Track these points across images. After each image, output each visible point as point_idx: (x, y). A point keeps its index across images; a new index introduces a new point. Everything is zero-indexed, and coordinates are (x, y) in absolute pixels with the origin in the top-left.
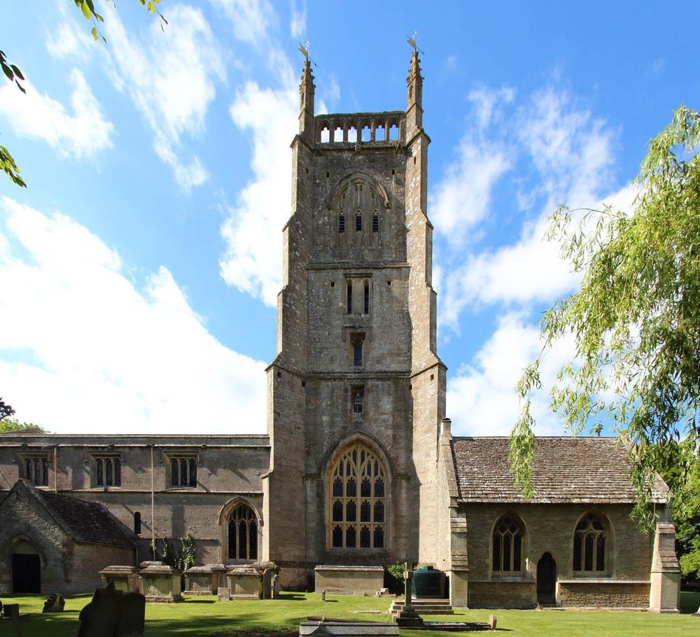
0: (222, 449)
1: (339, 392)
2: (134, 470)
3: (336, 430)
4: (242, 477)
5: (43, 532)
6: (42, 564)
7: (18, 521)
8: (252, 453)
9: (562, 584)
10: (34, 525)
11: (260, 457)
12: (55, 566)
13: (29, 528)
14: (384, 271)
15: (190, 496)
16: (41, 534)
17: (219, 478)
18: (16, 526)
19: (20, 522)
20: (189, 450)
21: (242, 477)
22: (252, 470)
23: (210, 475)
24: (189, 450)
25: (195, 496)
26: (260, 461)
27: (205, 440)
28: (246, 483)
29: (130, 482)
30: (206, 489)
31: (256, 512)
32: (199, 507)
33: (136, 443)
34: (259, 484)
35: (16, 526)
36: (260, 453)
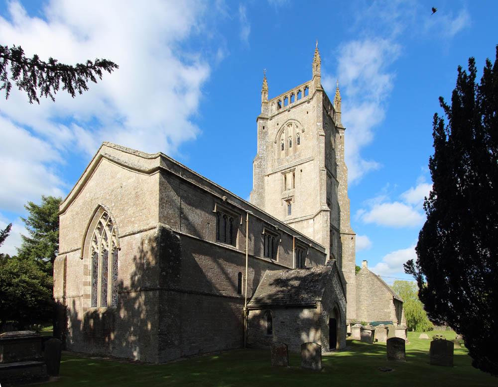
20: (304, 245)
30: (198, 236)
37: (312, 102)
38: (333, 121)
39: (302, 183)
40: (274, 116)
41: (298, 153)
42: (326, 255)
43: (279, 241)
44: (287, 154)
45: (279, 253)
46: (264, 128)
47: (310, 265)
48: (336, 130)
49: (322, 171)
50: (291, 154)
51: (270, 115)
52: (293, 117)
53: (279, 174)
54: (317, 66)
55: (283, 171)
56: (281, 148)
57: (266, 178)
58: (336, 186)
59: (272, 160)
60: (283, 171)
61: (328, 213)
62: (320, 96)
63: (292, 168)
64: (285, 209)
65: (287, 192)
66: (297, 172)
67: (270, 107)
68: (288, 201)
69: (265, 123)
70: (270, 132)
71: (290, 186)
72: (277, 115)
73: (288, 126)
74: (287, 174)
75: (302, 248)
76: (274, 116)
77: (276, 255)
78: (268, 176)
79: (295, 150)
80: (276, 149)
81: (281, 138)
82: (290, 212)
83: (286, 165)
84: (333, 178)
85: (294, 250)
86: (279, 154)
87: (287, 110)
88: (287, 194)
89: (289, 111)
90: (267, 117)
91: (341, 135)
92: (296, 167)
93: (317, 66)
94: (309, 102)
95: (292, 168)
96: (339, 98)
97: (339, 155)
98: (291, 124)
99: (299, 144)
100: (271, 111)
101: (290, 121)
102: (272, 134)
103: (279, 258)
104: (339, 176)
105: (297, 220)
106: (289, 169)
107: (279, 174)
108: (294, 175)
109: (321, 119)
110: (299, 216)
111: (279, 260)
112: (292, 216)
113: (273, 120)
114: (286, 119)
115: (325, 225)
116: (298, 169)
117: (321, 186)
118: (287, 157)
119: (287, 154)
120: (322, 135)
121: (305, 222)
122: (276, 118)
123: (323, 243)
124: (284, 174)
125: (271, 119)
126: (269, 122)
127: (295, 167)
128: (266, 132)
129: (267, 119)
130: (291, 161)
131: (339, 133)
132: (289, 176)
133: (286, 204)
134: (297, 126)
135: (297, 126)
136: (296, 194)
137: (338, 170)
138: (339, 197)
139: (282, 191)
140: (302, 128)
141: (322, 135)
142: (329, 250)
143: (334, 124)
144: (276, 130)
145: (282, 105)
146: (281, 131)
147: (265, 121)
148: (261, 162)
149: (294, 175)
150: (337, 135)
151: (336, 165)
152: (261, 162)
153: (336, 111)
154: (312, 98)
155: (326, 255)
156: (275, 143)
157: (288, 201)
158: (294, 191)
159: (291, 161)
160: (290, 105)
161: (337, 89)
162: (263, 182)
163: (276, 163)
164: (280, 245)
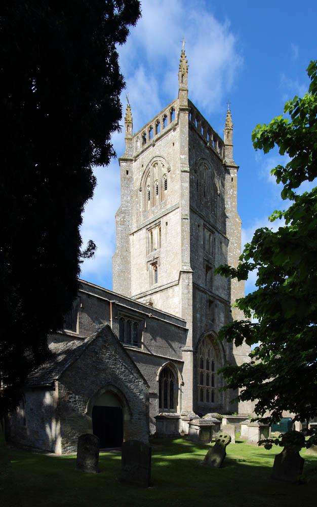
0: (160, 322)
1: (204, 301)
2: (92, 319)
3: (203, 325)
4: (171, 347)
5: (129, 385)
6: (126, 417)
7: (104, 370)
8: (176, 330)
9: (311, 425)
10: (121, 377)
11: (181, 335)
12: (139, 419)
13: (116, 378)
14: (220, 235)
15: (139, 354)
16: (127, 386)
17: (158, 344)
18: (103, 375)
19: (107, 372)
20: (138, 315)
21: (171, 347)
22: (177, 343)
23: (151, 340)
24: (138, 315)
25: (142, 355)
26: (180, 338)
27: (148, 309)
28: (173, 353)
29: (88, 330)
30: (149, 351)
31: (173, 371)
32: (144, 364)
33: (92, 292)
34: (181, 355)
35: (103, 375)
36: (180, 331)
37: (178, 129)
38: (219, 158)
39: (168, 240)
40: (138, 156)
41: (163, 202)
42: (186, 330)
43: (78, 306)
44: (153, 204)
45: (79, 322)
46: (127, 173)
47: (153, 341)
48: (226, 169)
49: (184, 220)
50: (157, 203)
51: (135, 154)
52: (158, 153)
53: (144, 230)
54: (183, 75)
55: (149, 226)
56: (147, 198)
57: (131, 237)
58: (223, 244)
59: (137, 213)
60: (149, 226)
61: (191, 276)
62: (185, 117)
63: (157, 222)
64: (151, 276)
65: (154, 252)
66: (163, 225)
67: (134, 145)
68: (154, 264)
69: (129, 166)
70: (135, 178)
71: (156, 245)
72: (142, 152)
73: (154, 166)
74: (153, 230)
75: (134, 318)
76: (138, 156)
77: (76, 323)
78: (133, 234)
79: (162, 199)
80: (141, 198)
81: (148, 184)
82: (156, 281)
83: (151, 218)
84: (216, 233)
85: (111, 319)
86: (145, 205)
87: (151, 145)
88: (153, 254)
89: (154, 146)
90: (130, 158)
91: (232, 175)
92: (161, 220)
93: (183, 75)
94: (175, 129)
95: (157, 222)
96: (231, 124)
97: (229, 203)
98: (157, 163)
99: (166, 188)
100: (136, 149)
101: (155, 159)
102: (137, 179)
103: (80, 328)
104: (228, 230)
105: (162, 288)
106: (154, 223)
107: (144, 230)
108: (160, 230)
109: (187, 149)
110: (165, 283)
111: (80, 332)
112: (159, 284)
113: (138, 160)
114: (150, 157)
115: (186, 291)
116: (163, 221)
117: (183, 239)
118: (153, 208)
119: (153, 204)
120: (184, 171)
121: (170, 290)
122: (141, 157)
123: (182, 316)
124: (150, 230)
125: (136, 160)
126: (134, 164)
127: (159, 220)
128: (131, 178)
129: (132, 160)
130: (157, 213)
131: (229, 173)
132: (156, 232)
133: (151, 268)
134: (163, 166)
135: (163, 166)
136: (162, 256)
137: (228, 223)
138: (229, 259)
139: (148, 252)
140: (166, 166)
141: (184, 171)
142: (192, 324)
143: (221, 161)
144: (141, 174)
145: (147, 137)
146: (146, 174)
147: (129, 163)
148: (124, 218)
149: (160, 230)
150: (227, 176)
151: (225, 217)
152: (124, 218)
153: (226, 142)
154: (177, 124)
155: (186, 330)
156: (141, 191)
157: (154, 264)
158: (160, 251)
159: (157, 213)
160: (155, 137)
161: (229, 113)
162: (128, 242)
163: (142, 218)
164: (82, 311)
